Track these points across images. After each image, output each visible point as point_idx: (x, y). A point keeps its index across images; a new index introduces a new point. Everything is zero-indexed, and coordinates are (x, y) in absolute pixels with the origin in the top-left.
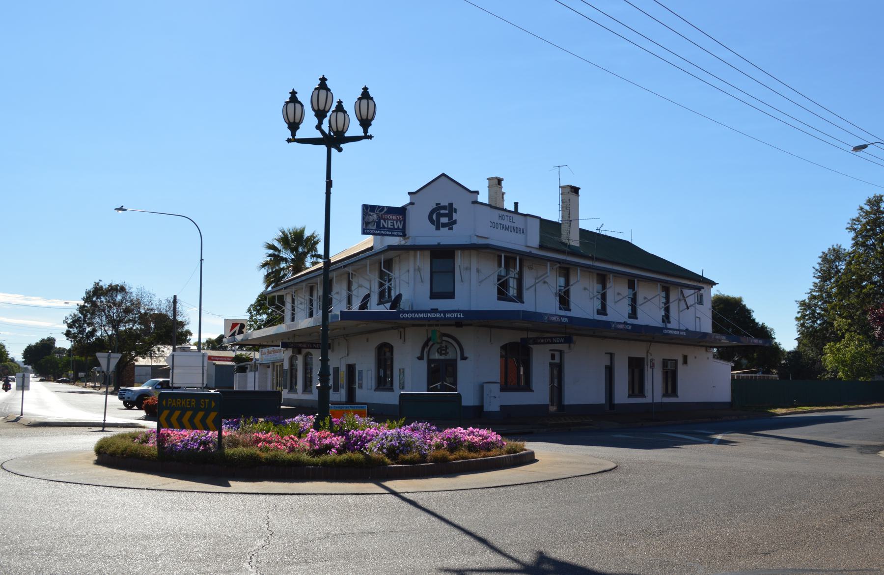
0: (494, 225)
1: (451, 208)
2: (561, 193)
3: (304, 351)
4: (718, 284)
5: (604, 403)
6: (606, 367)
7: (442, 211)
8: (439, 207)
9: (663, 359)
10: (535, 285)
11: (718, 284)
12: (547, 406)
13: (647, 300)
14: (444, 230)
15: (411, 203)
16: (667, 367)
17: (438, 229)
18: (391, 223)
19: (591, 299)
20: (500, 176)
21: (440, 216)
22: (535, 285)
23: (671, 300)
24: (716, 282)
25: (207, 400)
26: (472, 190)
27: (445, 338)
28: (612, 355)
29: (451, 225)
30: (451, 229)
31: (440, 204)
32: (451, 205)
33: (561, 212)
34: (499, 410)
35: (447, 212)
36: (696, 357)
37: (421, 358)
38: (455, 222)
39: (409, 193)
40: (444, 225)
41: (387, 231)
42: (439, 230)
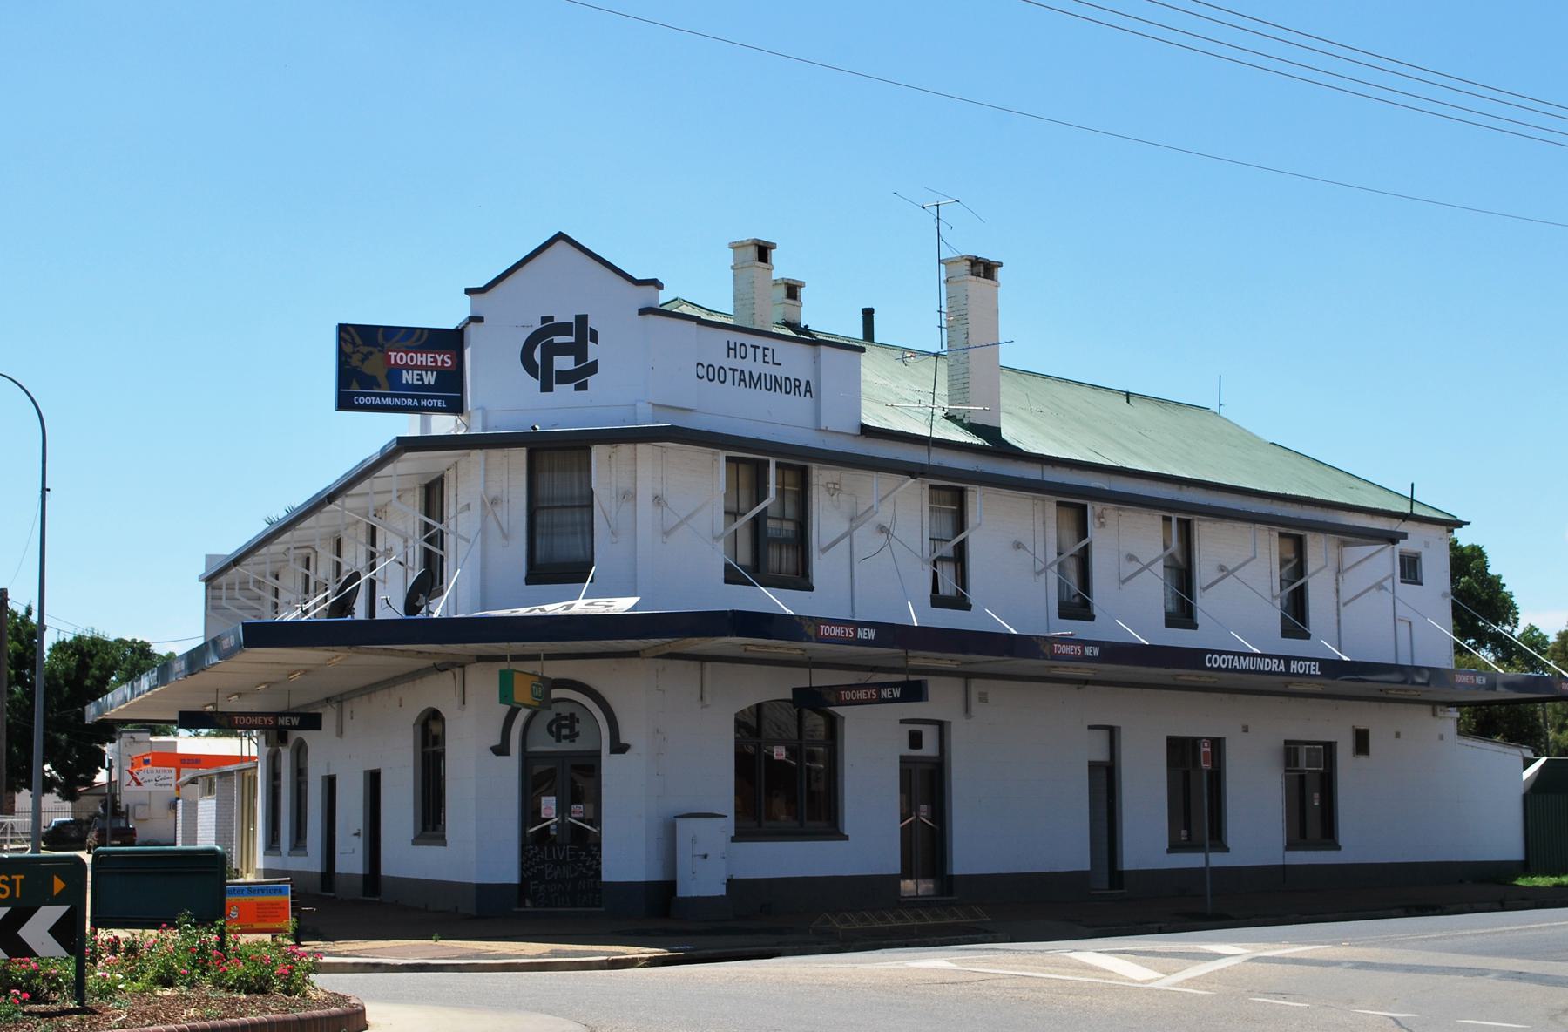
0: (713, 374)
1: (582, 330)
2: (943, 278)
3: (294, 735)
4: (1468, 523)
5: (1087, 867)
6: (1093, 766)
7: (558, 339)
8: (550, 326)
9: (1286, 742)
10: (849, 534)
11: (1468, 523)
12: (891, 882)
13: (1225, 573)
14: (564, 391)
15: (475, 319)
16: (1296, 764)
17: (546, 387)
18: (418, 375)
19: (1038, 573)
20: (766, 237)
21: (551, 351)
22: (849, 534)
23: (1311, 566)
24: (1460, 518)
25: (18, 878)
26: (482, 286)
27: (556, 693)
28: (1112, 732)
29: (581, 375)
30: (582, 387)
31: (551, 318)
32: (582, 320)
33: (944, 331)
34: (723, 893)
35: (572, 339)
36: (1398, 735)
37: (501, 750)
38: (593, 368)
39: (469, 291)
40: (564, 377)
41: (406, 397)
42: (551, 390)
